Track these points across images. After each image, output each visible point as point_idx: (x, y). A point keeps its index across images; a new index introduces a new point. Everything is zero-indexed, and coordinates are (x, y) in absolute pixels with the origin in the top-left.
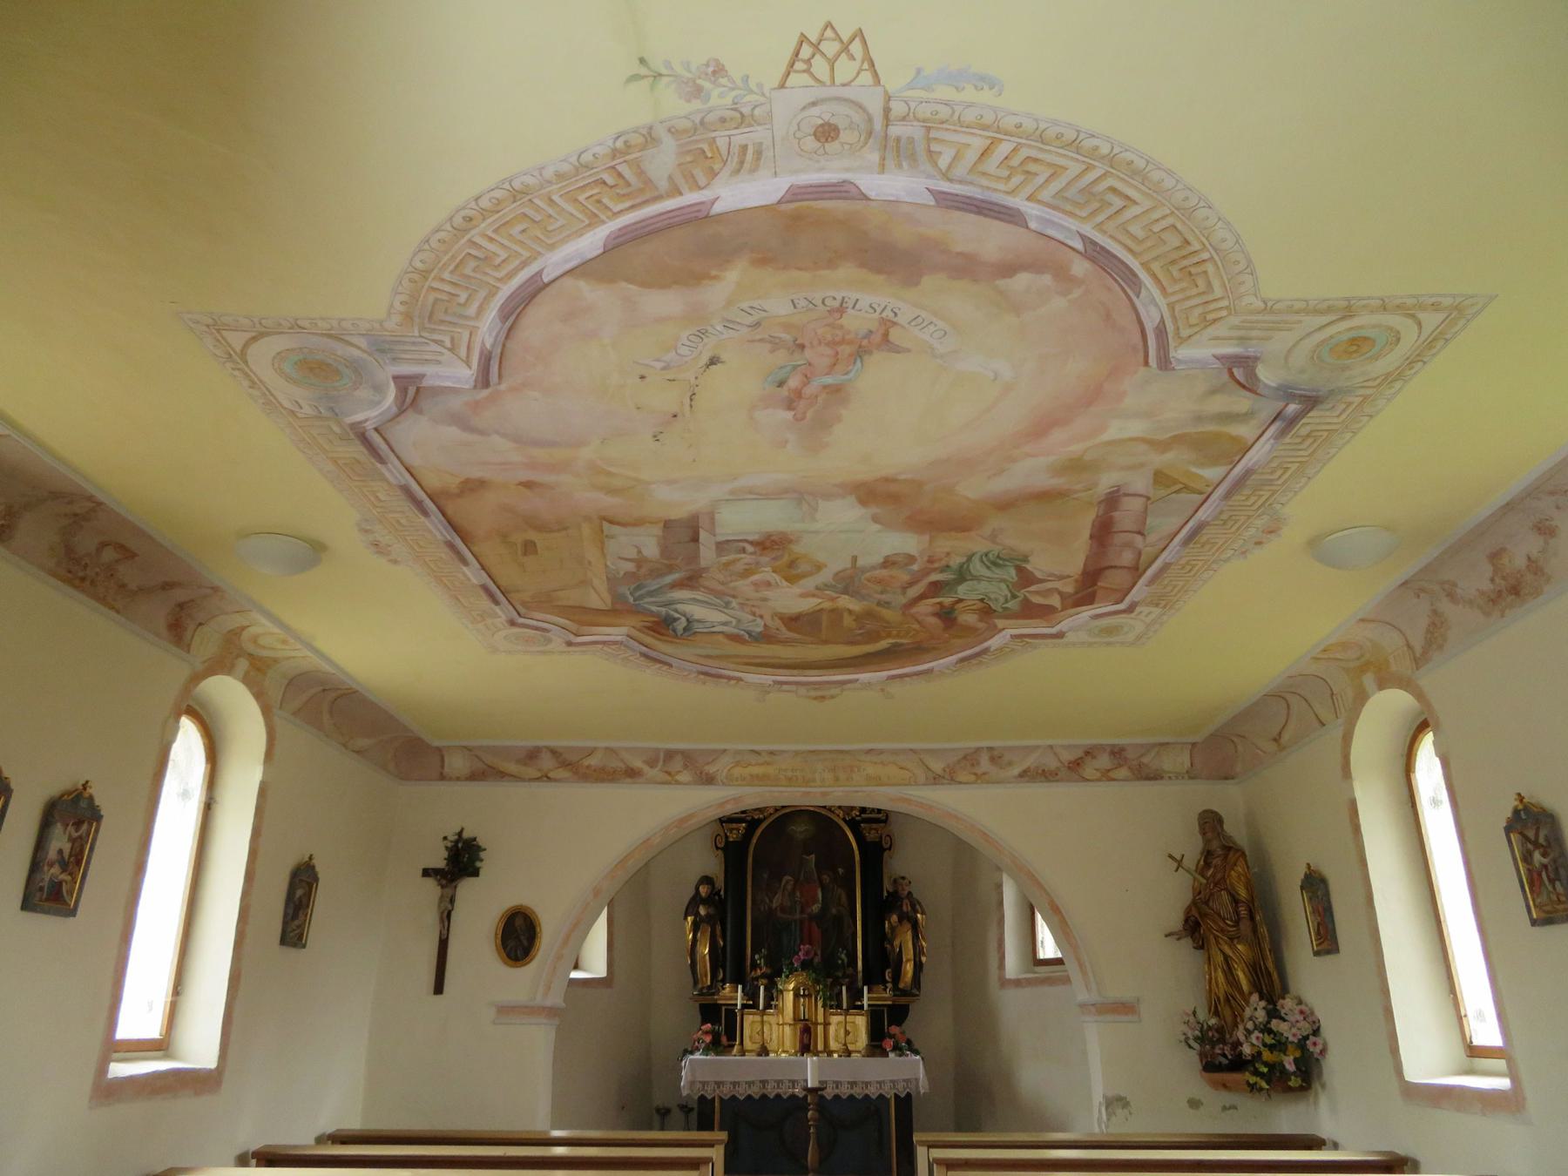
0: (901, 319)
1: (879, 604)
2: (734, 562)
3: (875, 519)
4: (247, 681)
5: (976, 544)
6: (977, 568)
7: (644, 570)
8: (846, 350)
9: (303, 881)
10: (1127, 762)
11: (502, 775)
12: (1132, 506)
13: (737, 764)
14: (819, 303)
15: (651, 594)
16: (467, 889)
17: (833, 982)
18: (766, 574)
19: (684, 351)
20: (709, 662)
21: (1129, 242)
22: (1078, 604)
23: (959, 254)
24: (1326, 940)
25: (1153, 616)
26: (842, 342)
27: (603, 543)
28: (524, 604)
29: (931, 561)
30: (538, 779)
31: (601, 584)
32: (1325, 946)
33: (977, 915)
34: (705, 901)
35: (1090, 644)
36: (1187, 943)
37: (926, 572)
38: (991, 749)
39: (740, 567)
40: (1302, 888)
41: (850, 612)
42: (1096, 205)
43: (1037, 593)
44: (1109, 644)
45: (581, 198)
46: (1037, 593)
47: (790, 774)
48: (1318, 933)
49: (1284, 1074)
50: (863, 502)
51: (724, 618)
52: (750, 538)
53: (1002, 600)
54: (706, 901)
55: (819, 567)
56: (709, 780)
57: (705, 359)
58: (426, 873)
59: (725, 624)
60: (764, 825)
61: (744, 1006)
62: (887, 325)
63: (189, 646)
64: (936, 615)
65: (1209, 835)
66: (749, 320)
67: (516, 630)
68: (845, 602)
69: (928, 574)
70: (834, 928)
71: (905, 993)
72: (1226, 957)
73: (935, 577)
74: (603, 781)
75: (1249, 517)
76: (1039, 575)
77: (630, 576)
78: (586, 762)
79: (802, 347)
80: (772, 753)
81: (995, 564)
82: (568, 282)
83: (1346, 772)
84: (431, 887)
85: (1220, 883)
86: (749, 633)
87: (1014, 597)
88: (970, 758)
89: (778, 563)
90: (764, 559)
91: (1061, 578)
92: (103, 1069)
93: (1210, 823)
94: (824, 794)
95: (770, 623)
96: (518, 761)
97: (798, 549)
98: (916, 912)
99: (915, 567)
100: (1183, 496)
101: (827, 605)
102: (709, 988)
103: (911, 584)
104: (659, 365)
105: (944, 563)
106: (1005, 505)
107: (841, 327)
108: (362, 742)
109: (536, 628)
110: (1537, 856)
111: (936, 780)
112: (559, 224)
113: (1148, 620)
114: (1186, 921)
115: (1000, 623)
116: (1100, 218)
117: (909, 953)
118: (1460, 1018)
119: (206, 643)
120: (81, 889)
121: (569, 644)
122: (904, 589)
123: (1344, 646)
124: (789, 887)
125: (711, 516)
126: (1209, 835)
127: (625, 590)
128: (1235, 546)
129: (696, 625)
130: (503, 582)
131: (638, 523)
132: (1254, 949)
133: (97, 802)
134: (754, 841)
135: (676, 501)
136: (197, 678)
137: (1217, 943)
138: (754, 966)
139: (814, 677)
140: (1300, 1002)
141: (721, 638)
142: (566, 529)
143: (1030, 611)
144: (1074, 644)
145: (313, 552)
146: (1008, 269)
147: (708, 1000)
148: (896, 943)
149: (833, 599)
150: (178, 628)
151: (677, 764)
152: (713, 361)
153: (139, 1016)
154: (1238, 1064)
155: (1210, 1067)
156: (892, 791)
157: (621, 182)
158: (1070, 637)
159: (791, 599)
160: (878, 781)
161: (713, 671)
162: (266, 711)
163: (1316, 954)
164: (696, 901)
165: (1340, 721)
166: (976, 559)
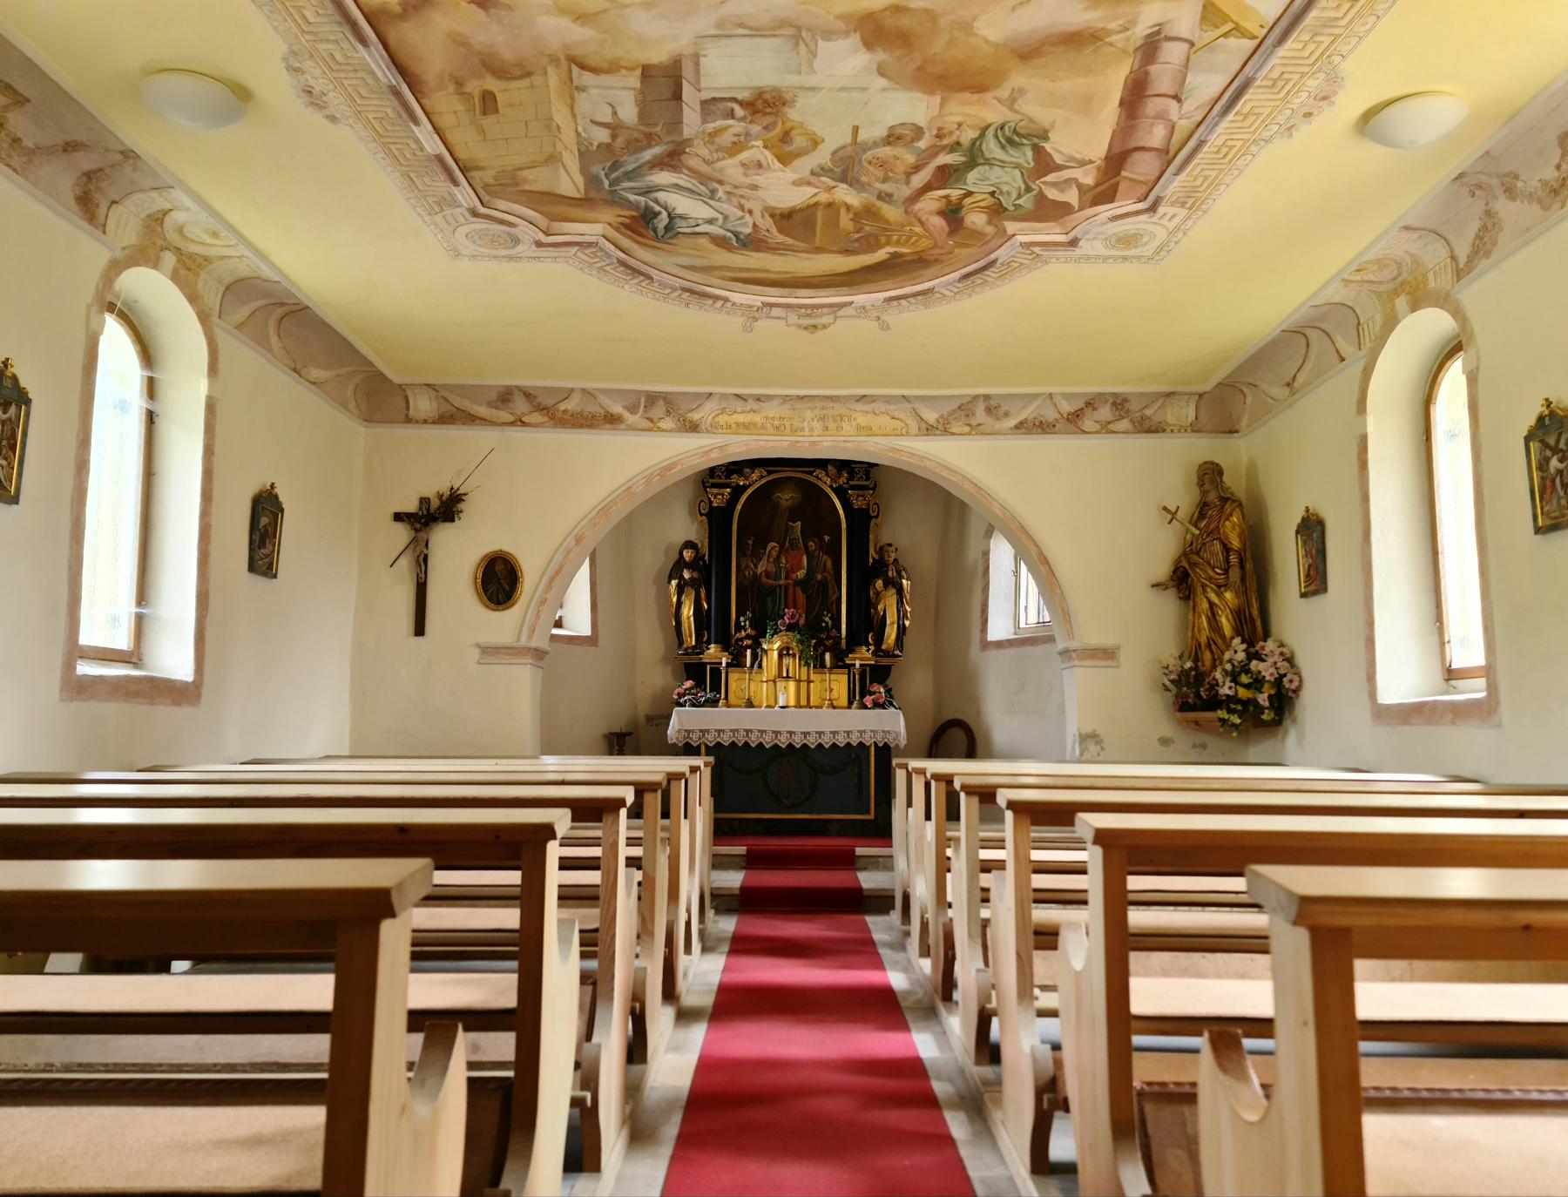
1: (879, 197)
3: (881, 71)
4: (175, 277)
5: (990, 111)
6: (991, 148)
7: (620, 142)
9: (266, 514)
10: (1131, 413)
11: (471, 419)
12: (1172, 54)
13: (723, 411)
15: (629, 175)
16: (443, 538)
17: (820, 647)
18: (757, 151)
22: (1096, 202)
24: (1316, 580)
25: (1177, 221)
27: (572, 98)
28: (486, 186)
29: (939, 136)
30: (512, 424)
31: (572, 161)
32: (1312, 587)
33: (962, 585)
34: (689, 566)
35: (1105, 259)
36: (1171, 593)
37: (934, 151)
38: (987, 397)
39: (726, 139)
40: (1297, 532)
41: (848, 207)
43: (1054, 185)
44: (1125, 258)
46: (1054, 185)
47: (777, 423)
48: (1308, 575)
49: (1260, 709)
50: (869, 45)
51: (707, 213)
52: (740, 97)
53: (1015, 195)
54: (689, 566)
55: (815, 143)
56: (694, 428)
58: (398, 517)
59: (711, 222)
60: (750, 491)
61: (728, 665)
63: (104, 226)
64: (941, 213)
65: (1207, 486)
67: (480, 225)
68: (845, 194)
69: (936, 155)
70: (819, 594)
71: (887, 654)
72: (1212, 605)
73: (945, 159)
74: (581, 426)
75: (1303, 75)
76: (1058, 159)
77: (606, 148)
78: (562, 406)
80: (758, 399)
81: (1010, 141)
83: (1361, 407)
84: (402, 533)
85: (1213, 533)
86: (736, 235)
87: (1028, 190)
88: (965, 408)
89: (772, 134)
90: (755, 129)
91: (1083, 163)
92: (69, 666)
93: (1210, 474)
94: (813, 443)
95: (760, 221)
96: (489, 404)
97: (793, 114)
98: (901, 577)
99: (922, 144)
100: (1232, 41)
101: (824, 197)
102: (694, 648)
103: (917, 168)
105: (954, 138)
106: (1029, 52)
108: (316, 373)
109: (502, 222)
110: (1554, 463)
111: (929, 430)
113: (1171, 225)
114: (1174, 572)
115: (1011, 227)
117: (891, 617)
118: (1442, 644)
119: (125, 224)
120: (20, 475)
121: (539, 244)
122: (908, 175)
123: (1380, 263)
124: (774, 553)
125: (696, 59)
126: (1207, 486)
127: (598, 170)
128: (1281, 119)
130: (462, 154)
131: (613, 68)
132: (1234, 624)
133: (23, 384)
134: (739, 507)
135: (656, 36)
136: (116, 267)
137: (1204, 591)
138: (739, 628)
139: (805, 298)
140: (1282, 645)
142: (529, 74)
143: (1047, 211)
144: (1088, 258)
145: (239, 97)
147: (693, 659)
148: (880, 607)
149: (829, 189)
150: (88, 203)
151: (659, 410)
153: (105, 619)
154: (1214, 703)
155: (1183, 706)
156: (883, 441)
158: (1085, 247)
159: (784, 187)
160: (868, 431)
162: (204, 318)
163: (1303, 595)
164: (680, 564)
165: (1363, 352)
166: (990, 133)
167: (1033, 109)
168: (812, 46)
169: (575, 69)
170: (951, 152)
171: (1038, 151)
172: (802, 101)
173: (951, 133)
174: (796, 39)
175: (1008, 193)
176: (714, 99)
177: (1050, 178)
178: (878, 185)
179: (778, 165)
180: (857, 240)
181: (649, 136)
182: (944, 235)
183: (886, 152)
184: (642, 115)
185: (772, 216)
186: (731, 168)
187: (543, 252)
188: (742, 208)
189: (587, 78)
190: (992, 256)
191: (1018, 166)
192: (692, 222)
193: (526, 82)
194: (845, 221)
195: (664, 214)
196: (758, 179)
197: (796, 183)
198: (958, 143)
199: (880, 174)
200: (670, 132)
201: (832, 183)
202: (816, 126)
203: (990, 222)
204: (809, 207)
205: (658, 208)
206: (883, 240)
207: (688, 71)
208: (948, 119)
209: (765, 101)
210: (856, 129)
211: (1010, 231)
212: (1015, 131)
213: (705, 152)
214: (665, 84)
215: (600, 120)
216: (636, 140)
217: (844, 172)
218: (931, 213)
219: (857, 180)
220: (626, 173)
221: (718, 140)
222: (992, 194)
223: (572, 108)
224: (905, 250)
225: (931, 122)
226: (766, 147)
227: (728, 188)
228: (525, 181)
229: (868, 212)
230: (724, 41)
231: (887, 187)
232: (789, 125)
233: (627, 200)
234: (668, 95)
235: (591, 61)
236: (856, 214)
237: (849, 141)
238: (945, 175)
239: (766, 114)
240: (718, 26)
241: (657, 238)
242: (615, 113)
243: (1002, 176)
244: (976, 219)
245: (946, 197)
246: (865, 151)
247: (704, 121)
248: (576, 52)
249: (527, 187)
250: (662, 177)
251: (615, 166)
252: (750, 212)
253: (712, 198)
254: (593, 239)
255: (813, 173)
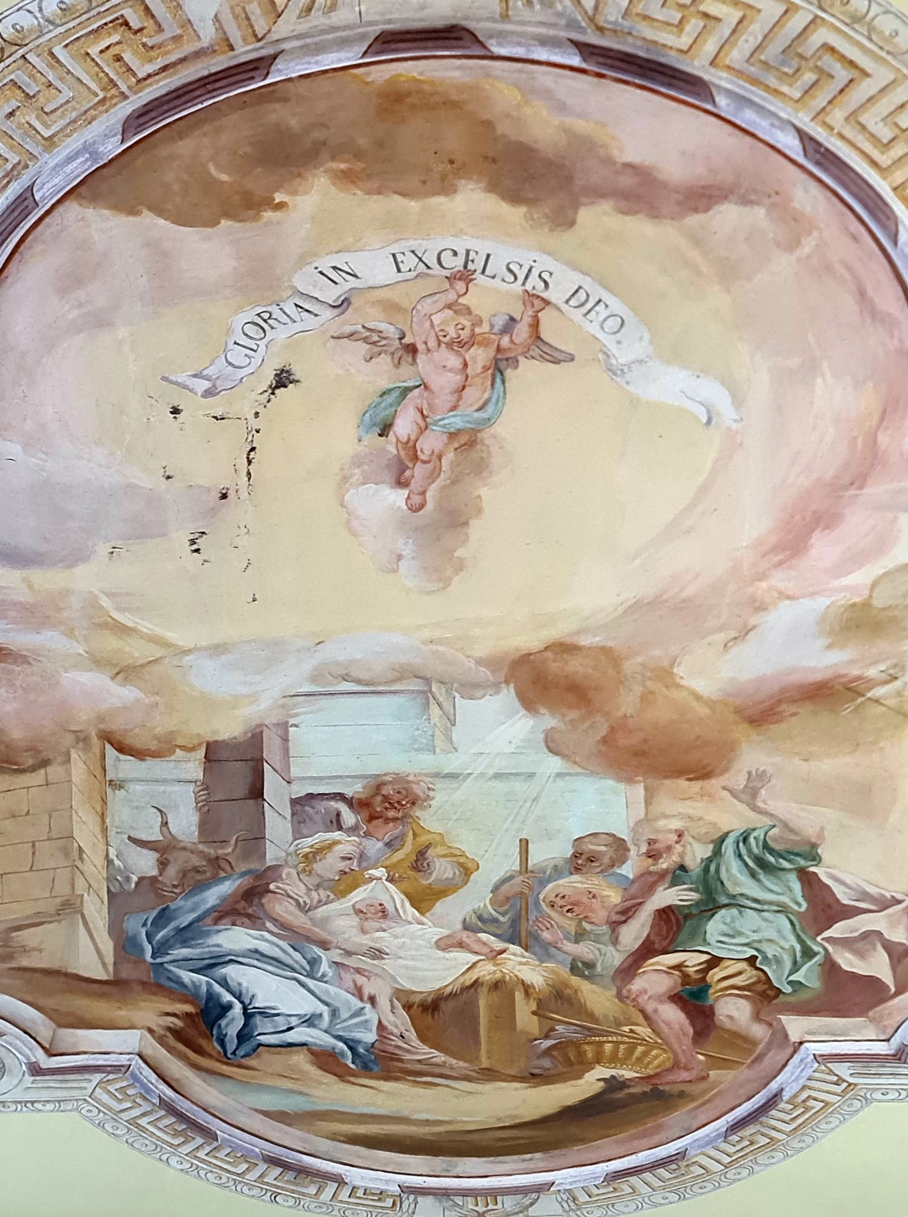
0: (555, 295)
2: (336, 843)
3: (552, 745)
6: (735, 876)
7: (172, 872)
8: (479, 357)
14: (433, 263)
15: (185, 935)
18: (379, 889)
19: (237, 356)
20: (291, 1136)
21: (868, 148)
23: (628, 165)
26: (471, 341)
29: (653, 855)
31: (96, 910)
37: (649, 882)
39: (330, 865)
41: (527, 989)
42: (809, 77)
45: (94, 51)
50: (528, 703)
51: (306, 1004)
52: (349, 792)
53: (788, 965)
55: (467, 870)
57: (269, 378)
59: (310, 1021)
62: (537, 302)
64: (676, 998)
66: (332, 294)
68: (519, 965)
69: (650, 889)
73: (668, 896)
76: (843, 896)
77: (150, 883)
79: (412, 350)
82: (73, 209)
86: (352, 1044)
87: (808, 954)
89: (399, 855)
90: (374, 847)
95: (389, 1020)
97: (429, 819)
99: (628, 870)
101: (486, 971)
103: (627, 913)
104: (203, 385)
106: (764, 711)
107: (468, 311)
112: (62, 99)
116: (821, 100)
121: (36, 1070)
125: (284, 727)
127: (136, 925)
129: (261, 1025)
131: (161, 750)
135: (229, 702)
141: (300, 1059)
142: (45, 763)
146: (701, 197)
152: (283, 379)
157: (149, 24)
159: (424, 955)
161: (293, 1158)
166: (728, 848)
167: (791, 807)
168: (448, 707)
169: (110, 751)
170: (673, 884)
171: (808, 880)
172: (441, 797)
173: (669, 848)
174: (426, 697)
175: (778, 961)
176: (311, 796)
177: (838, 930)
178: (569, 946)
179: (411, 912)
180: (548, 1051)
181: (216, 862)
182: (687, 1041)
183: (573, 883)
184: (205, 825)
185: (408, 1007)
186: (339, 917)
187: (51, 1088)
188: (358, 992)
189: (123, 766)
190: (774, 1086)
191: (783, 909)
192: (282, 1023)
193: (38, 777)
194: (525, 1016)
195: (238, 1007)
196: (384, 939)
197: (445, 944)
198: (682, 868)
199: (571, 926)
200: (246, 855)
201: (499, 945)
202: (467, 843)
203: (757, 1017)
204: (465, 989)
205: (227, 997)
206: (589, 1051)
207: (271, 751)
208: (662, 823)
209: (386, 798)
210: (524, 844)
211: (794, 1037)
212: (766, 846)
213: (298, 889)
214: (238, 770)
215: (144, 837)
216: (196, 870)
217: (515, 923)
218: (659, 999)
219: (537, 938)
220: (180, 931)
221: (318, 867)
222: (751, 960)
223: (103, 817)
224: (627, 1074)
225: (634, 830)
226: (390, 880)
227: (335, 955)
228: (24, 950)
229: (557, 1000)
230: (324, 702)
231: (584, 950)
232: (424, 839)
233: (179, 982)
234: (241, 790)
235: (138, 740)
236: (540, 1002)
237: (515, 864)
238: (673, 927)
239: (387, 820)
240: (314, 678)
241: (225, 1058)
242: (165, 824)
243: (753, 931)
244: (734, 1011)
245: (679, 967)
246: (543, 883)
247: (298, 835)
248: (116, 725)
249: (25, 962)
250: (234, 938)
251: (164, 917)
252: (372, 1000)
253: (311, 976)
254: (123, 1060)
255: (467, 927)
